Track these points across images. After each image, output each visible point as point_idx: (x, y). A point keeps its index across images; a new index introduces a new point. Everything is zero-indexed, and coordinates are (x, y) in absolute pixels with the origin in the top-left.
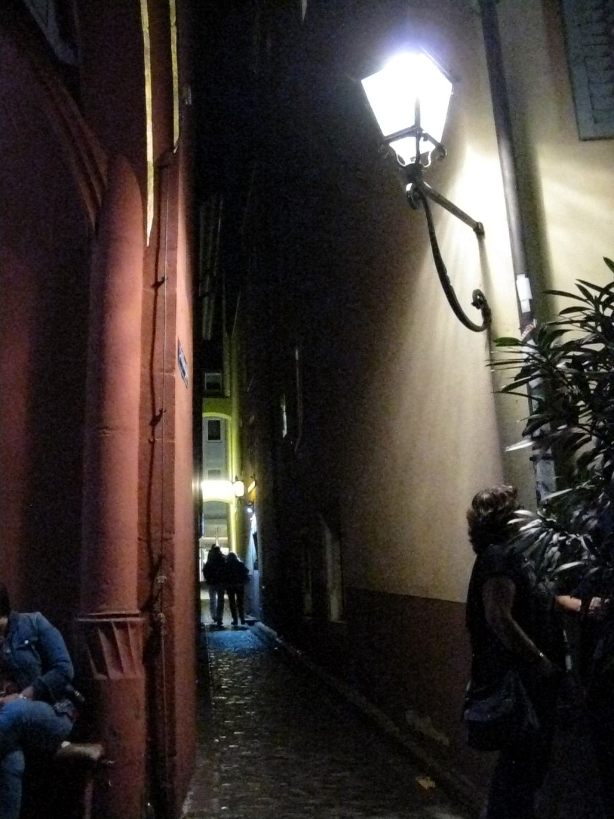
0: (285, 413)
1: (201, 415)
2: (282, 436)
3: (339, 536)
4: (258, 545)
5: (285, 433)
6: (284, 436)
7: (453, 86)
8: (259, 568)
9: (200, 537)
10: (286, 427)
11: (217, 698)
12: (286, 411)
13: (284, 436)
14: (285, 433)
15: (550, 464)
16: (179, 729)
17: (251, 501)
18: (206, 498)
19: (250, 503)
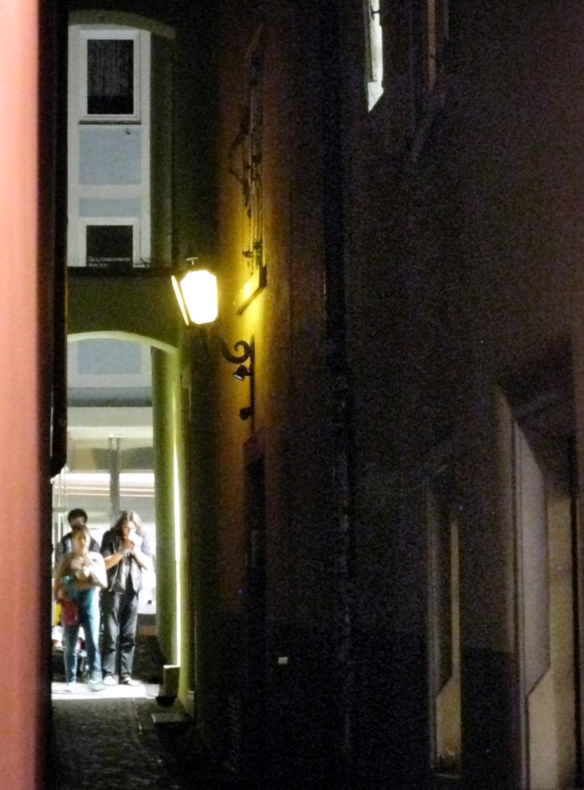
0: (377, 17)
1: (60, 508)
2: (366, 103)
3: (189, 421)
4: (524, 773)
5: (375, 91)
6: (370, 108)
7: (218, 279)
8: (136, 617)
9: (57, 471)
10: (378, 71)
11: (66, 285)
12: (53, 424)
13: (370, 108)
14: (375, 91)
15: (54, 482)
16: (114, 338)
17: (243, 343)
18: (66, 479)
19: (241, 352)
